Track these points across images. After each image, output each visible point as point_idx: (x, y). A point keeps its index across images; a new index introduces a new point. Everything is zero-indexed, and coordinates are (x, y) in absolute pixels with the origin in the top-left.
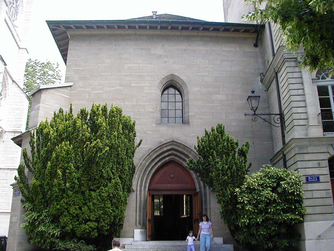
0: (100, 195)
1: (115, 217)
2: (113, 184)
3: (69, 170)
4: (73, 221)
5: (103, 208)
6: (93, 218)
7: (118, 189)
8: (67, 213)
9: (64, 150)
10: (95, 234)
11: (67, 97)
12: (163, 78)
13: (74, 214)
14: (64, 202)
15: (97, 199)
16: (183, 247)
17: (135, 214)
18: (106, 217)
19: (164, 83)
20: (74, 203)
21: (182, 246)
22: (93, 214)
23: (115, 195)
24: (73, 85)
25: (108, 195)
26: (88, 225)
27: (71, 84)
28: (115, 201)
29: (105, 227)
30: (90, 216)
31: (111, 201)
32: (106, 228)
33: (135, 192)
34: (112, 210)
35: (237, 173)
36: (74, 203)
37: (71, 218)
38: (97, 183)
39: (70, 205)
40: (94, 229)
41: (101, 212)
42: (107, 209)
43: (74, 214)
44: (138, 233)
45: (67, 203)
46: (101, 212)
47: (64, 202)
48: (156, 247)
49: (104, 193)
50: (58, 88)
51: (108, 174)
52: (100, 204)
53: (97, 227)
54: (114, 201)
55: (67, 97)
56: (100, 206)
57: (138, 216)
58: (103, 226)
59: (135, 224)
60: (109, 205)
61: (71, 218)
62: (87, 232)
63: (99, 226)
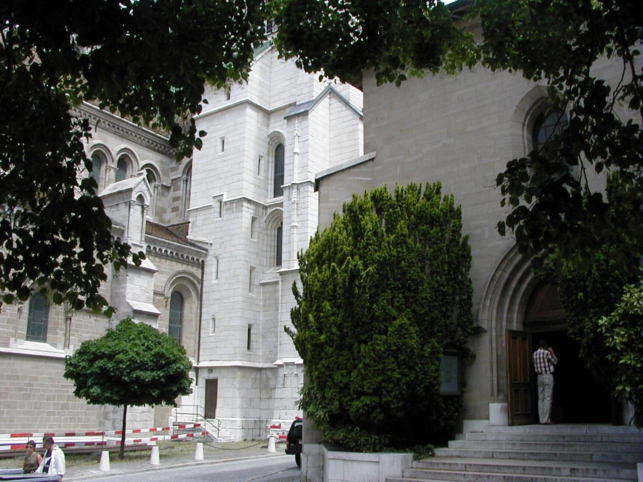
0: (374, 350)
1: (411, 385)
2: (395, 327)
3: (324, 312)
4: (342, 395)
5: (383, 372)
6: (368, 388)
7: (406, 336)
8: (331, 382)
9: (318, 281)
10: (378, 416)
11: (368, 179)
12: (522, 100)
13: (341, 385)
14: (323, 365)
15: (371, 356)
16: (568, 439)
17: (489, 375)
18: (391, 386)
19: (527, 109)
20: (339, 366)
21: (567, 436)
22: (368, 383)
23: (402, 346)
24: (375, 156)
25: (386, 348)
26: (362, 402)
27: (372, 155)
28: (402, 358)
29: (394, 404)
30: (363, 386)
31: (396, 358)
32: (396, 406)
33: (488, 334)
34: (400, 373)
35: (603, 284)
36: (339, 366)
37: (338, 390)
38: (370, 329)
39: (333, 370)
40: (374, 408)
41: (380, 378)
42: (389, 373)
43: (341, 385)
44: (496, 411)
45: (328, 367)
46: (380, 378)
47: (323, 365)
48: (519, 438)
49: (380, 345)
50: (349, 168)
51: (385, 311)
52: (376, 364)
53: (380, 403)
54: (401, 357)
55: (368, 179)
56: (377, 368)
57: (495, 379)
58: (389, 402)
59: (489, 391)
60: (394, 366)
61: (338, 390)
62: (363, 414)
63: (382, 403)
